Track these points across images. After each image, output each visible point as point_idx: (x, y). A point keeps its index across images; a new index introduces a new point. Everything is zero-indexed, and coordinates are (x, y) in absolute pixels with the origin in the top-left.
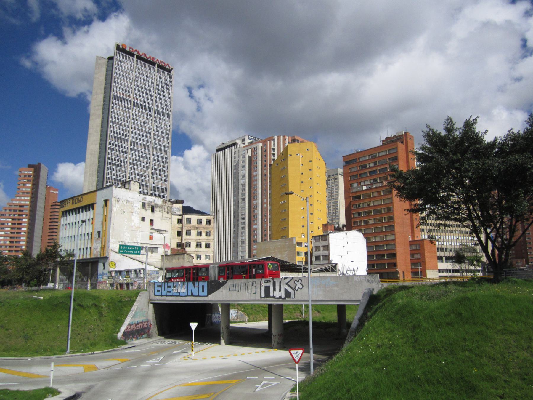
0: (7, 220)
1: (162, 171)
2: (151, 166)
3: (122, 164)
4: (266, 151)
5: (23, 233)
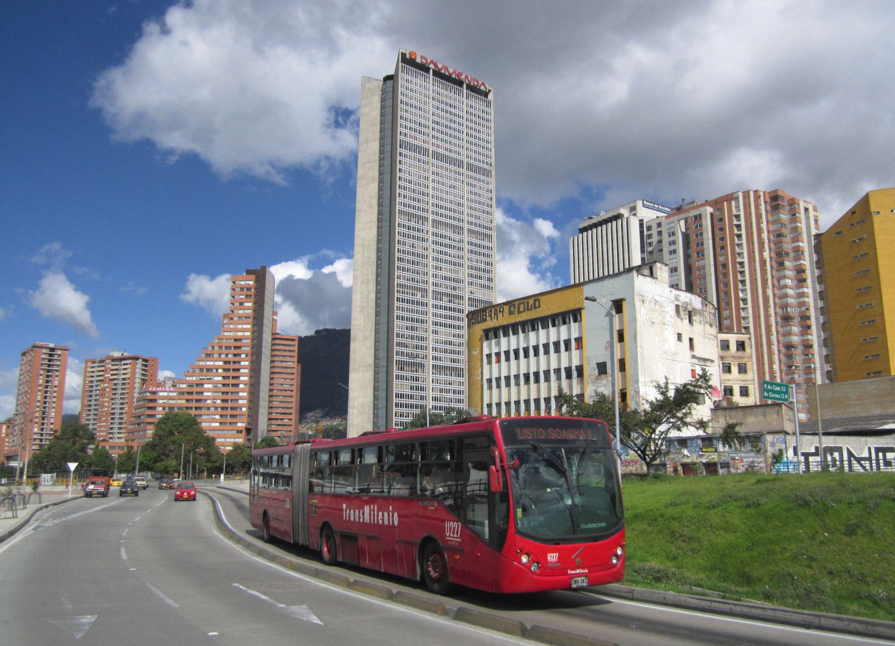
0: (217, 363)
1: (484, 271)
2: (467, 263)
3: (420, 260)
4: (721, 220)
5: (242, 386)
